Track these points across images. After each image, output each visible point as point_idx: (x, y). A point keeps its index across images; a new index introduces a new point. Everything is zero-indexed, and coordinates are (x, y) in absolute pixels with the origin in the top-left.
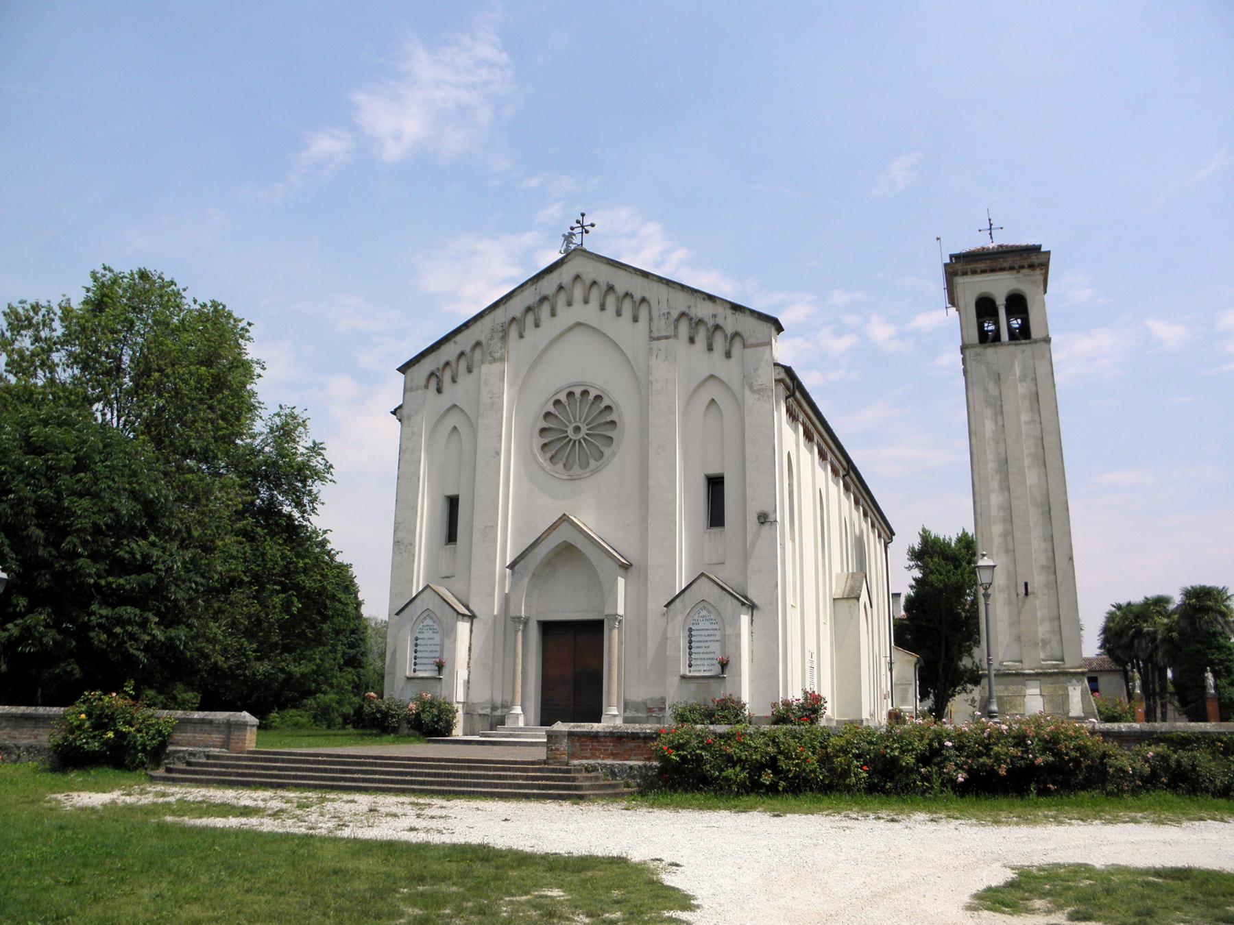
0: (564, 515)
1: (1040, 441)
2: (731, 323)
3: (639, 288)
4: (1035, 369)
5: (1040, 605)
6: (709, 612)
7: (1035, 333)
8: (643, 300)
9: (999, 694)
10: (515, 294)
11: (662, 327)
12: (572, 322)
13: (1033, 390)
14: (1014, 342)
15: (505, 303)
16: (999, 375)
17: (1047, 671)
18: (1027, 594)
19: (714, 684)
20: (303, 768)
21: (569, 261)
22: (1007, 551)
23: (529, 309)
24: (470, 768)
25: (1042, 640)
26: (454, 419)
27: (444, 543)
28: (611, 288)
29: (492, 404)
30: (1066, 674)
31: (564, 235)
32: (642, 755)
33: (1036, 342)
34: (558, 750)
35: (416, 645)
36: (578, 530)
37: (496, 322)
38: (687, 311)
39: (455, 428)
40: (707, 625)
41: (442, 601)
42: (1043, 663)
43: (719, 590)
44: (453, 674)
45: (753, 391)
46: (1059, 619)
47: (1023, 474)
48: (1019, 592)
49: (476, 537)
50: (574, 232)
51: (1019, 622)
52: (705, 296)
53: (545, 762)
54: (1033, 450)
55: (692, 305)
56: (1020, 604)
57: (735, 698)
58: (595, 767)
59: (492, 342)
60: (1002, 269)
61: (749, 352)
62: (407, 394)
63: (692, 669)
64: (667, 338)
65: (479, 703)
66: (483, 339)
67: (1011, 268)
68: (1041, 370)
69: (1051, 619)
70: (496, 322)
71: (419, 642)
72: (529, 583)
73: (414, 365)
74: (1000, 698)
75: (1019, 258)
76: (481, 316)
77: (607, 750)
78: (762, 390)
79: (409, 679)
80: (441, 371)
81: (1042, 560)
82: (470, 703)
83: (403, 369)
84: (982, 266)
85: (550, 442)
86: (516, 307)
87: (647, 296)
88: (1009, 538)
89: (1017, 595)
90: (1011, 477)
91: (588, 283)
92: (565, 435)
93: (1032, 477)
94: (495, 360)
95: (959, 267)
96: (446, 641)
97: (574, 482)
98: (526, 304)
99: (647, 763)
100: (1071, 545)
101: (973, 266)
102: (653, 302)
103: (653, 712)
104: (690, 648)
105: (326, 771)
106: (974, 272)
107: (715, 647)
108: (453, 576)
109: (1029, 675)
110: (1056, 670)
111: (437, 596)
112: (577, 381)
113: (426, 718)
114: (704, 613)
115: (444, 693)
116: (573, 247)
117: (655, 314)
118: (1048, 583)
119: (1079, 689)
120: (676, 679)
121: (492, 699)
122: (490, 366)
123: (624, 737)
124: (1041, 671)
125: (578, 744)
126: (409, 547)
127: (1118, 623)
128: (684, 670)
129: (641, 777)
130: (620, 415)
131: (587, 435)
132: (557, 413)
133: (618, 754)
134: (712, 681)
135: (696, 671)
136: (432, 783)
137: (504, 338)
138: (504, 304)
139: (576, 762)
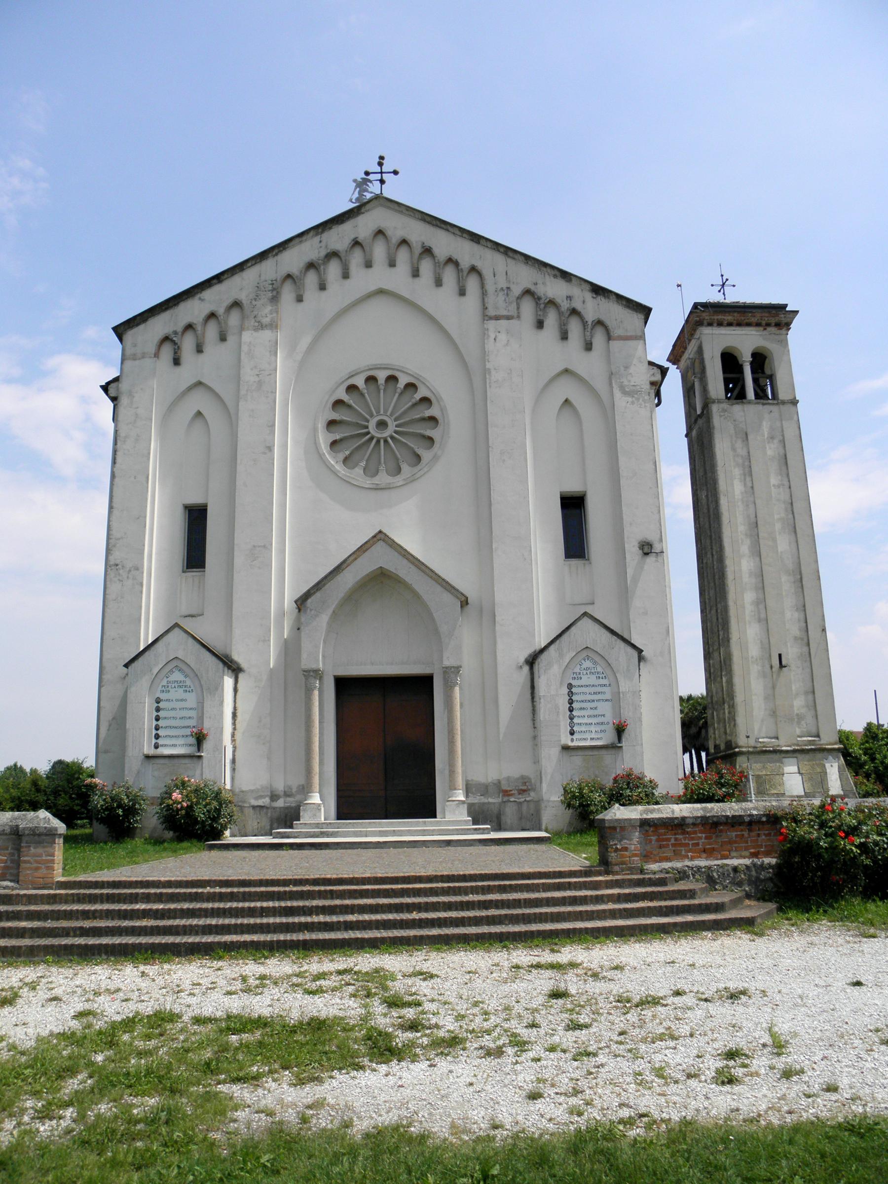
0: (380, 532)
1: (790, 506)
2: (592, 308)
3: (466, 253)
4: (783, 431)
5: (795, 677)
6: (595, 663)
7: (782, 395)
8: (473, 269)
9: (757, 773)
10: (291, 244)
11: (498, 304)
12: (373, 288)
13: (782, 452)
14: (759, 401)
15: (277, 254)
16: (746, 434)
17: (804, 747)
18: (781, 666)
19: (608, 757)
20: (206, 910)
21: (368, 210)
22: (760, 621)
23: (311, 266)
24: (503, 889)
25: (797, 715)
26: (198, 401)
27: (181, 569)
28: (427, 251)
29: (260, 383)
30: (824, 750)
31: (355, 181)
32: (746, 849)
33: (783, 403)
34: (626, 849)
35: (158, 709)
36: (400, 553)
37: (263, 278)
38: (533, 288)
39: (199, 414)
40: (593, 680)
41: (198, 646)
42: (799, 739)
43: (608, 634)
44: (219, 748)
45: (625, 393)
46: (814, 692)
47: (774, 540)
48: (773, 664)
49: (239, 560)
50: (371, 177)
51: (774, 696)
52: (558, 273)
53: (587, 873)
54: (783, 515)
55: (540, 282)
56: (775, 676)
57: (636, 772)
58: (685, 872)
59: (258, 303)
60: (749, 325)
61: (615, 345)
62: (128, 363)
63: (575, 737)
64: (508, 318)
65: (252, 791)
66: (243, 297)
67: (758, 325)
68: (789, 434)
69: (806, 693)
70: (263, 278)
71: (161, 705)
72: (330, 624)
73: (138, 325)
74: (758, 777)
75: (767, 315)
76: (240, 267)
77: (698, 844)
78: (637, 392)
79: (148, 757)
80: (179, 336)
81: (795, 630)
82: (237, 790)
83: (120, 331)
84: (729, 318)
85: (341, 440)
86: (292, 260)
87: (479, 264)
88: (762, 606)
89: (771, 667)
90: (761, 542)
91: (395, 240)
92: (365, 431)
93: (784, 544)
94: (261, 327)
95: (706, 316)
96: (207, 704)
97: (379, 492)
98: (307, 259)
99: (756, 860)
100: (824, 616)
101: (720, 317)
102: (487, 273)
103: (512, 795)
104: (571, 710)
105: (252, 912)
106: (720, 324)
107: (605, 709)
108: (200, 615)
109: (787, 752)
110: (813, 747)
111: (191, 640)
112: (378, 362)
113: (200, 814)
114: (587, 664)
115: (208, 775)
116: (368, 196)
117: (490, 287)
118: (801, 654)
119: (836, 765)
120: (555, 751)
121: (271, 785)
122: (255, 334)
123: (721, 824)
124: (799, 748)
125: (654, 838)
126: (133, 572)
127: (687, 713)
128: (566, 740)
129: (750, 882)
130: (443, 410)
131: (396, 432)
132: (351, 402)
133: (713, 849)
134: (603, 752)
135: (580, 739)
136: (477, 921)
137: (275, 299)
138: (274, 256)
139: (654, 867)
